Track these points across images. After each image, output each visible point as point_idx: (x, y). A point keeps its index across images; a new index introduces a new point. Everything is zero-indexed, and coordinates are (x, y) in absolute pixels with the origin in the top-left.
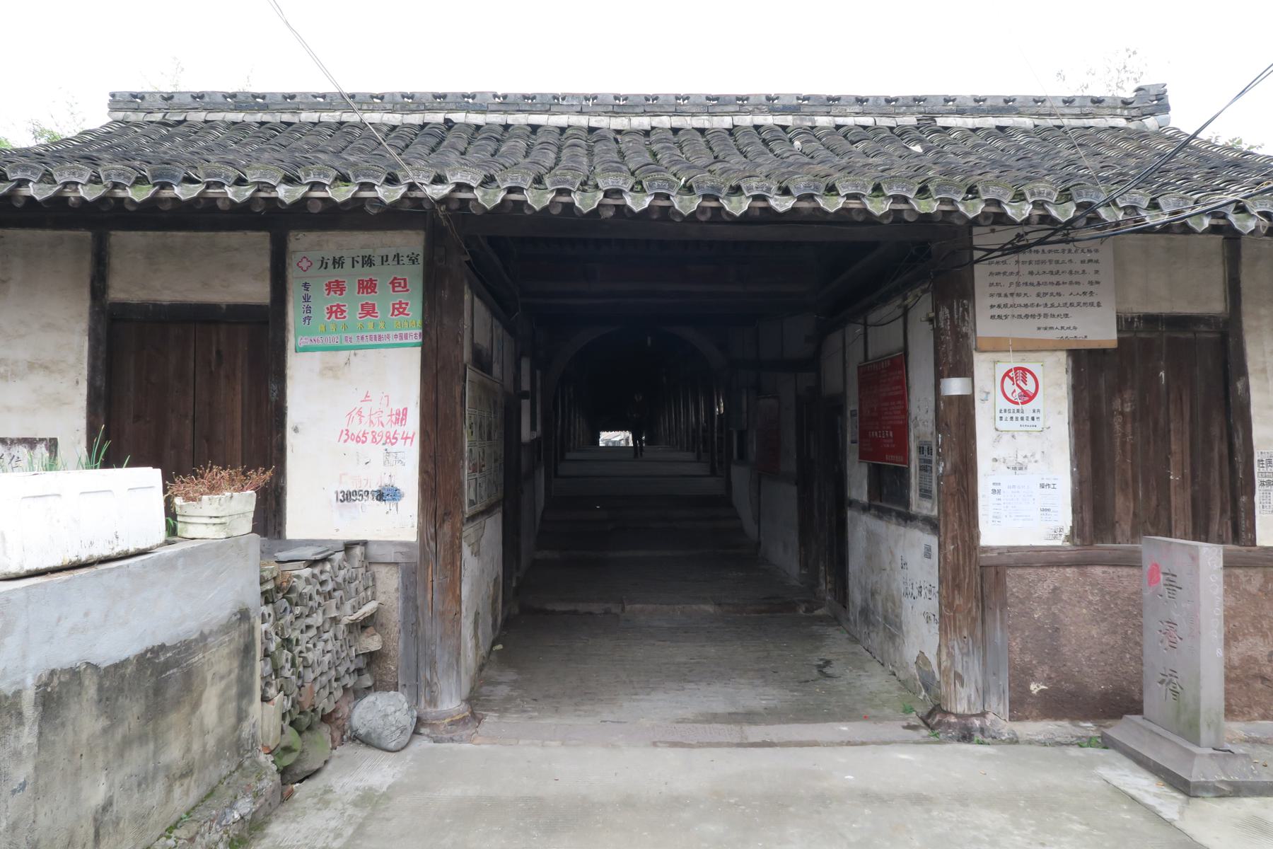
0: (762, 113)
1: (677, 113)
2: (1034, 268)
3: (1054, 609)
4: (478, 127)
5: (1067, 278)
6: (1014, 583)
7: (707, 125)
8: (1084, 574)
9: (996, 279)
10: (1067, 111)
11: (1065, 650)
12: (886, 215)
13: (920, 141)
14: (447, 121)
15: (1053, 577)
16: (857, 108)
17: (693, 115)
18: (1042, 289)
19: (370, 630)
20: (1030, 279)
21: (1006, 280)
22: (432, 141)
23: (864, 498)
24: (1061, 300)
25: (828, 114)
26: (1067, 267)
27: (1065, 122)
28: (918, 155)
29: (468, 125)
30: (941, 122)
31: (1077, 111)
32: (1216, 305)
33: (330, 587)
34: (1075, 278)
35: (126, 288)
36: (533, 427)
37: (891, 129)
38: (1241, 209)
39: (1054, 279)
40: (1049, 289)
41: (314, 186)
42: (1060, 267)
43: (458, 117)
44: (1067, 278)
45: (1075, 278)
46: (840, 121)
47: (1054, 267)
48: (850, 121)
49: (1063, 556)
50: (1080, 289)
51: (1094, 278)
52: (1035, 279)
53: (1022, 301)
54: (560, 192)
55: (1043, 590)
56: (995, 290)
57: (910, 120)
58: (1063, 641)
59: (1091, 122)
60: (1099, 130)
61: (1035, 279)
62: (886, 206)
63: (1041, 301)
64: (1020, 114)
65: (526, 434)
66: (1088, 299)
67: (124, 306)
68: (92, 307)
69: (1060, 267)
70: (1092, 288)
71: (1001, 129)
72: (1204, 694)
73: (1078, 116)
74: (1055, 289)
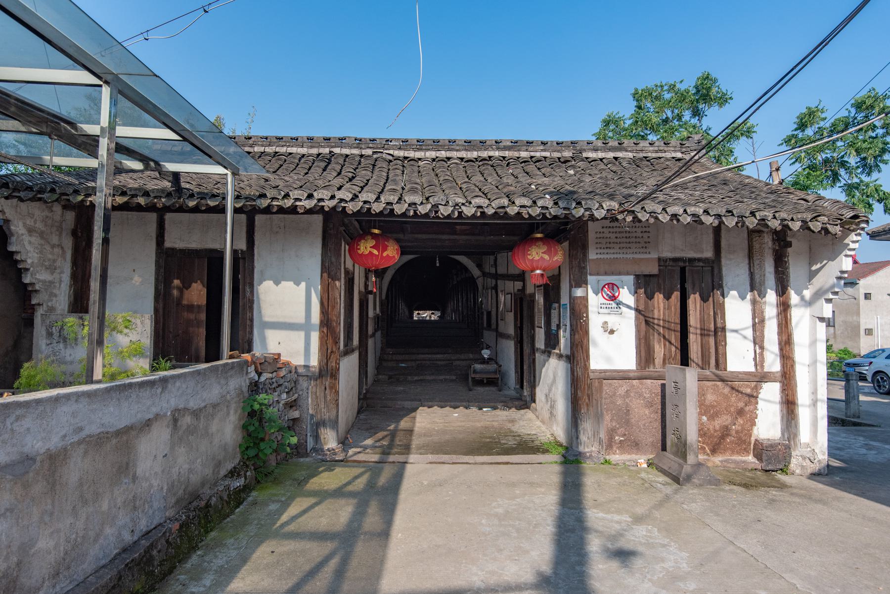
0: (493, 150)
1: (449, 150)
2: (618, 235)
3: (627, 400)
4: (347, 156)
5: (634, 240)
6: (608, 387)
7: (465, 156)
8: (641, 384)
9: (599, 241)
10: (651, 149)
11: (633, 421)
12: (539, 215)
13: (573, 167)
14: (331, 152)
15: (623, 387)
16: (542, 147)
17: (457, 151)
18: (622, 245)
19: (294, 408)
20: (615, 240)
21: (604, 241)
22: (323, 164)
23: (543, 347)
24: (631, 251)
25: (527, 150)
26: (634, 235)
27: (649, 155)
28: (571, 176)
29: (342, 155)
30: (585, 155)
31: (656, 149)
32: (709, 254)
33: (275, 385)
34: (638, 240)
35: (173, 241)
36: (375, 309)
37: (559, 158)
38: (706, 212)
39: (628, 240)
40: (624, 245)
41: (273, 199)
42: (631, 235)
43: (337, 150)
44: (634, 240)
45: (638, 240)
46: (532, 154)
47: (628, 235)
48: (538, 154)
49: (632, 375)
50: (641, 245)
51: (647, 240)
52: (618, 240)
53: (612, 251)
54: (388, 204)
55: (622, 391)
56: (599, 246)
57: (567, 154)
58: (631, 416)
59: (663, 155)
60: (667, 160)
61: (618, 240)
62: (538, 211)
63: (621, 251)
64: (627, 151)
65: (371, 314)
66: (645, 250)
67: (173, 249)
68: (157, 250)
69: (631, 235)
70: (647, 245)
71: (616, 158)
72: (689, 438)
73: (656, 152)
74: (628, 245)
